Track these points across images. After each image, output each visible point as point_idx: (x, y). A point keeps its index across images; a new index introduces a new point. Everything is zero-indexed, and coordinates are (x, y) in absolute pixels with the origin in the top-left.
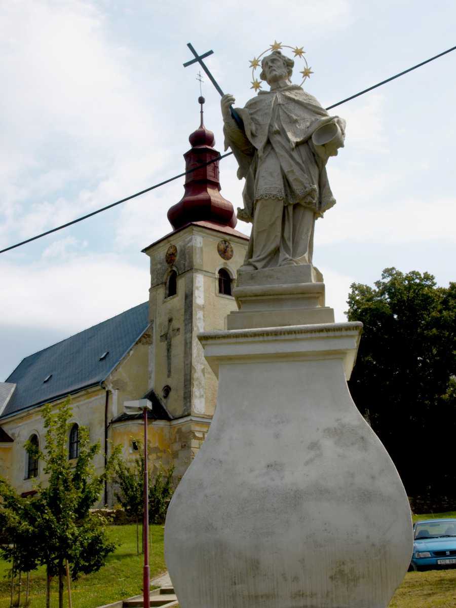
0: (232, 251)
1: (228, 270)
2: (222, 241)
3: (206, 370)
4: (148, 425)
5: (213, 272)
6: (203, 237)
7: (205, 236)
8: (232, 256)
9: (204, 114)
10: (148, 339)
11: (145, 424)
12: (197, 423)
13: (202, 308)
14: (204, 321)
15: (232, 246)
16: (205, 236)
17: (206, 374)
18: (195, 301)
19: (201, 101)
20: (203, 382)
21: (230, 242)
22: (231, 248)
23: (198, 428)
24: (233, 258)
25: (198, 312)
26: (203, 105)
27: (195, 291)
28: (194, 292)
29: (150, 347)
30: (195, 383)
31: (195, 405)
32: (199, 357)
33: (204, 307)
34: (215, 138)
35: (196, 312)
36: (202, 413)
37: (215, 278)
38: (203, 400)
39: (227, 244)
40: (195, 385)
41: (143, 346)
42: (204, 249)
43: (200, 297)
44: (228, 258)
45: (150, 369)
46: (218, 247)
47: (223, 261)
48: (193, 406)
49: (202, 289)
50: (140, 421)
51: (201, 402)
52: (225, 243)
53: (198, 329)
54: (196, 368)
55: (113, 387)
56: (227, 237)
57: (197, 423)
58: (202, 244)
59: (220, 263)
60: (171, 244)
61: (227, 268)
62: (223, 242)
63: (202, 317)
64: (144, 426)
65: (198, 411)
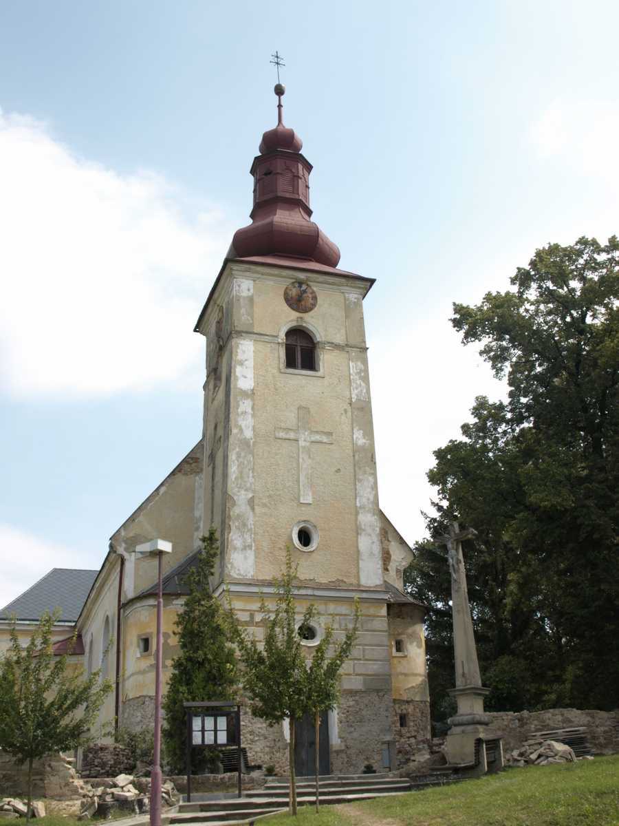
0: (315, 298)
1: (308, 329)
2: (293, 283)
3: (256, 501)
4: (164, 607)
5: (275, 334)
6: (254, 281)
7: (259, 278)
8: (314, 305)
9: (282, 109)
10: (193, 465)
11: (158, 606)
12: (239, 595)
13: (251, 394)
14: (253, 416)
15: (315, 289)
16: (259, 278)
17: (256, 507)
18: (236, 385)
19: (279, 91)
20: (251, 522)
21: (309, 283)
22: (313, 292)
23: (237, 604)
24: (316, 309)
25: (241, 403)
26: (282, 97)
27: (235, 367)
28: (232, 371)
29: (197, 478)
30: (234, 525)
31: (232, 564)
32: (242, 477)
33: (254, 394)
34: (295, 131)
35: (238, 402)
36: (249, 576)
37: (279, 343)
38: (251, 554)
39: (304, 287)
40: (233, 528)
41: (184, 478)
42: (256, 299)
43: (245, 377)
44: (306, 310)
45: (197, 514)
46: (286, 294)
47: (295, 315)
48: (229, 566)
49: (250, 363)
50: (152, 602)
51: (246, 558)
52: (300, 287)
53: (241, 430)
54: (235, 498)
55: (126, 550)
56: (302, 276)
57: (239, 595)
58: (252, 291)
59: (289, 318)
60: (218, 306)
61: (304, 325)
62: (297, 285)
63: (250, 411)
64: (156, 609)
65: (240, 574)
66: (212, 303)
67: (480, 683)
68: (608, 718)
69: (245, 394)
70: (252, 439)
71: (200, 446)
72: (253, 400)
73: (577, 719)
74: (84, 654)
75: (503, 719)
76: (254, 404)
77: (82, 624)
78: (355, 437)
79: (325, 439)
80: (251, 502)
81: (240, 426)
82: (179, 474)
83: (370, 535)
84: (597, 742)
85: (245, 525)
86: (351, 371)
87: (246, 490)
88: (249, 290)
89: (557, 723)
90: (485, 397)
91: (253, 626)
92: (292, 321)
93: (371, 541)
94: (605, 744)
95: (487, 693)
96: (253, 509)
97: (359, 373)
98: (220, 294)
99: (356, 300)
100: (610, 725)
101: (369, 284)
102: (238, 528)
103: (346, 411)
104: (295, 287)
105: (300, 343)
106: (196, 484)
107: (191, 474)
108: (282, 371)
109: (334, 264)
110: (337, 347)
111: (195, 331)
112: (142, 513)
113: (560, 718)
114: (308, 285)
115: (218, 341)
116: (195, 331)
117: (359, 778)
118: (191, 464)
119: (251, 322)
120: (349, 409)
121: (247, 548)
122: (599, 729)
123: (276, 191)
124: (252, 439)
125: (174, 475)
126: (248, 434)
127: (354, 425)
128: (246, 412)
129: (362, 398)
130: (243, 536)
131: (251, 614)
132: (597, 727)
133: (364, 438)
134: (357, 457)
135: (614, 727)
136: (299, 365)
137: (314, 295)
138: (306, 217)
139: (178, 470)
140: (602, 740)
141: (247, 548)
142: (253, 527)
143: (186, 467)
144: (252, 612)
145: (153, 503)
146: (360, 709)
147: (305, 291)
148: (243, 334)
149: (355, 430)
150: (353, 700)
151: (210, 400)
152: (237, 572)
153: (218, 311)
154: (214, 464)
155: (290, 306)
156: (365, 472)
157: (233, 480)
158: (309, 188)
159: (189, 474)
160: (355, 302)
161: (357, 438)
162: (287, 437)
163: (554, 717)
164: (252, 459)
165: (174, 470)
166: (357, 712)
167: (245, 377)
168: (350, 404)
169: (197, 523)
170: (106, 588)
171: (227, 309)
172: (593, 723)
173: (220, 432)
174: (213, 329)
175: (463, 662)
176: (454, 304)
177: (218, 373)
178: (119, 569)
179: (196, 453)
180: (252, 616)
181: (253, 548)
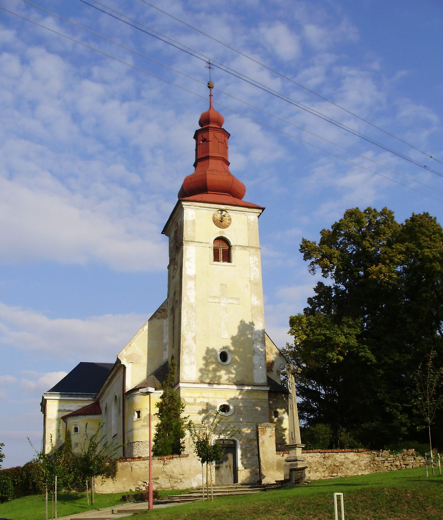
0: (230, 220)
13: (194, 278)
21: (227, 211)
29: (165, 321)
33: (195, 277)
43: (191, 268)
44: (225, 227)
46: (214, 218)
53: (189, 298)
59: (217, 232)
63: (193, 287)
66: (172, 220)
67: (301, 443)
68: (368, 457)
69: (191, 278)
70: (194, 303)
71: (166, 302)
72: (195, 281)
73: (352, 457)
74: (101, 414)
75: (315, 457)
76: (195, 283)
77: (99, 397)
78: (252, 300)
79: (235, 302)
80: (194, 339)
81: (188, 296)
82: (155, 319)
83: (260, 355)
84: (360, 468)
85: (191, 351)
86: (251, 263)
87: (192, 332)
88: (192, 216)
89: (342, 459)
90: (370, 207)
91: (196, 405)
92: (217, 233)
93: (260, 359)
94: (364, 469)
95: (304, 447)
96: (195, 342)
97: (255, 263)
98: (176, 217)
99: (254, 220)
100: (367, 460)
101: (261, 210)
102: (187, 353)
103: (247, 286)
104: (218, 213)
105: (222, 247)
106: (164, 324)
107: (162, 318)
108: (212, 263)
109: (241, 199)
110: (243, 247)
111: (162, 233)
112: (134, 341)
113: (343, 457)
114: (226, 212)
115: (176, 243)
116: (162, 233)
117: (225, 489)
118: (161, 313)
119: (194, 235)
120: (249, 284)
121: (192, 364)
122: (362, 462)
123: (209, 152)
124: (194, 303)
125: (152, 319)
126: (192, 300)
127: (252, 293)
128: (191, 288)
129: (256, 278)
130: (190, 357)
131: (195, 399)
132: (361, 461)
133: (257, 301)
134: (253, 312)
135: (370, 461)
136: (222, 260)
137: (230, 217)
138: (225, 165)
139: (154, 316)
140: (363, 468)
141: (192, 364)
142: (195, 352)
143: (159, 314)
144: (195, 398)
145: (140, 335)
146: (252, 449)
147: (224, 216)
148: (189, 243)
149: (252, 296)
150: (249, 444)
151: (171, 277)
152: (187, 377)
153: (175, 225)
154: (174, 315)
155: (216, 225)
156: (257, 320)
157: (185, 326)
158: (228, 148)
159: (160, 318)
160: (253, 221)
161: (253, 301)
162: (214, 301)
163: (340, 457)
164: (195, 314)
165: (152, 316)
166: (251, 450)
167: (191, 268)
168: (250, 281)
169: (165, 346)
170: (115, 380)
171: (180, 227)
172: (359, 459)
173: (177, 298)
174: (173, 235)
175: (292, 432)
176: (303, 238)
177: (176, 262)
178: (123, 370)
179: (164, 307)
180: (195, 400)
181: (196, 364)
